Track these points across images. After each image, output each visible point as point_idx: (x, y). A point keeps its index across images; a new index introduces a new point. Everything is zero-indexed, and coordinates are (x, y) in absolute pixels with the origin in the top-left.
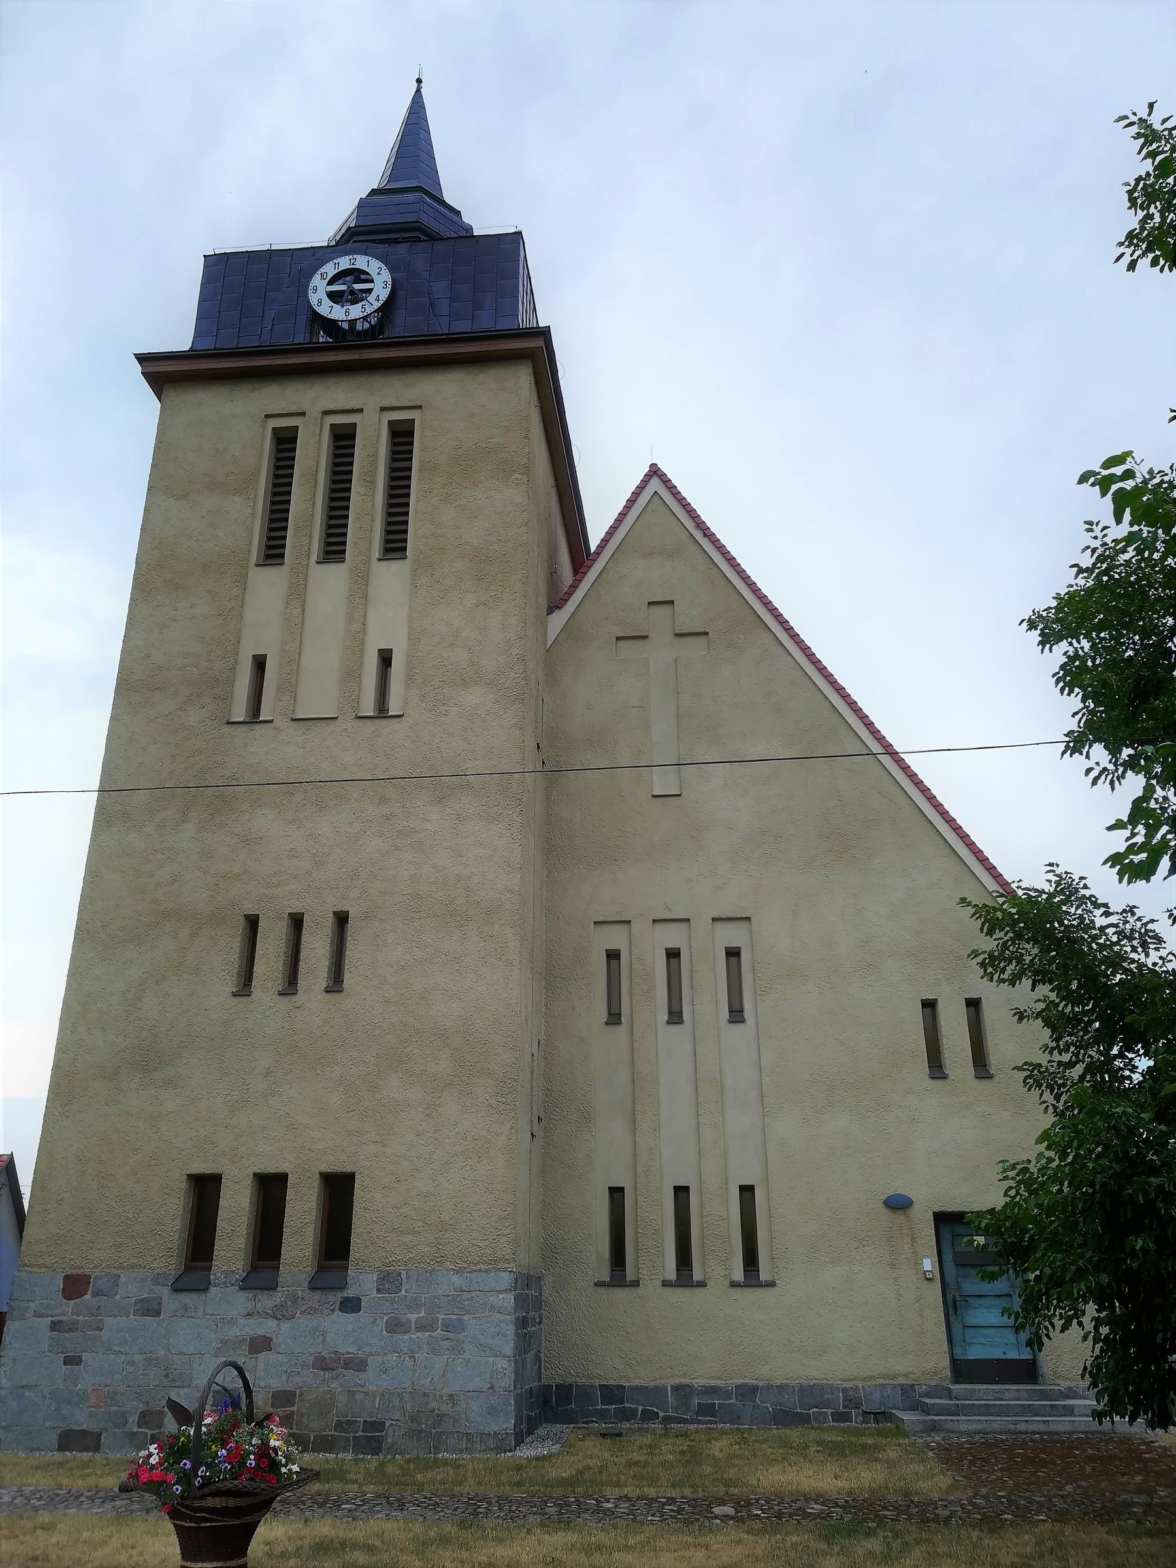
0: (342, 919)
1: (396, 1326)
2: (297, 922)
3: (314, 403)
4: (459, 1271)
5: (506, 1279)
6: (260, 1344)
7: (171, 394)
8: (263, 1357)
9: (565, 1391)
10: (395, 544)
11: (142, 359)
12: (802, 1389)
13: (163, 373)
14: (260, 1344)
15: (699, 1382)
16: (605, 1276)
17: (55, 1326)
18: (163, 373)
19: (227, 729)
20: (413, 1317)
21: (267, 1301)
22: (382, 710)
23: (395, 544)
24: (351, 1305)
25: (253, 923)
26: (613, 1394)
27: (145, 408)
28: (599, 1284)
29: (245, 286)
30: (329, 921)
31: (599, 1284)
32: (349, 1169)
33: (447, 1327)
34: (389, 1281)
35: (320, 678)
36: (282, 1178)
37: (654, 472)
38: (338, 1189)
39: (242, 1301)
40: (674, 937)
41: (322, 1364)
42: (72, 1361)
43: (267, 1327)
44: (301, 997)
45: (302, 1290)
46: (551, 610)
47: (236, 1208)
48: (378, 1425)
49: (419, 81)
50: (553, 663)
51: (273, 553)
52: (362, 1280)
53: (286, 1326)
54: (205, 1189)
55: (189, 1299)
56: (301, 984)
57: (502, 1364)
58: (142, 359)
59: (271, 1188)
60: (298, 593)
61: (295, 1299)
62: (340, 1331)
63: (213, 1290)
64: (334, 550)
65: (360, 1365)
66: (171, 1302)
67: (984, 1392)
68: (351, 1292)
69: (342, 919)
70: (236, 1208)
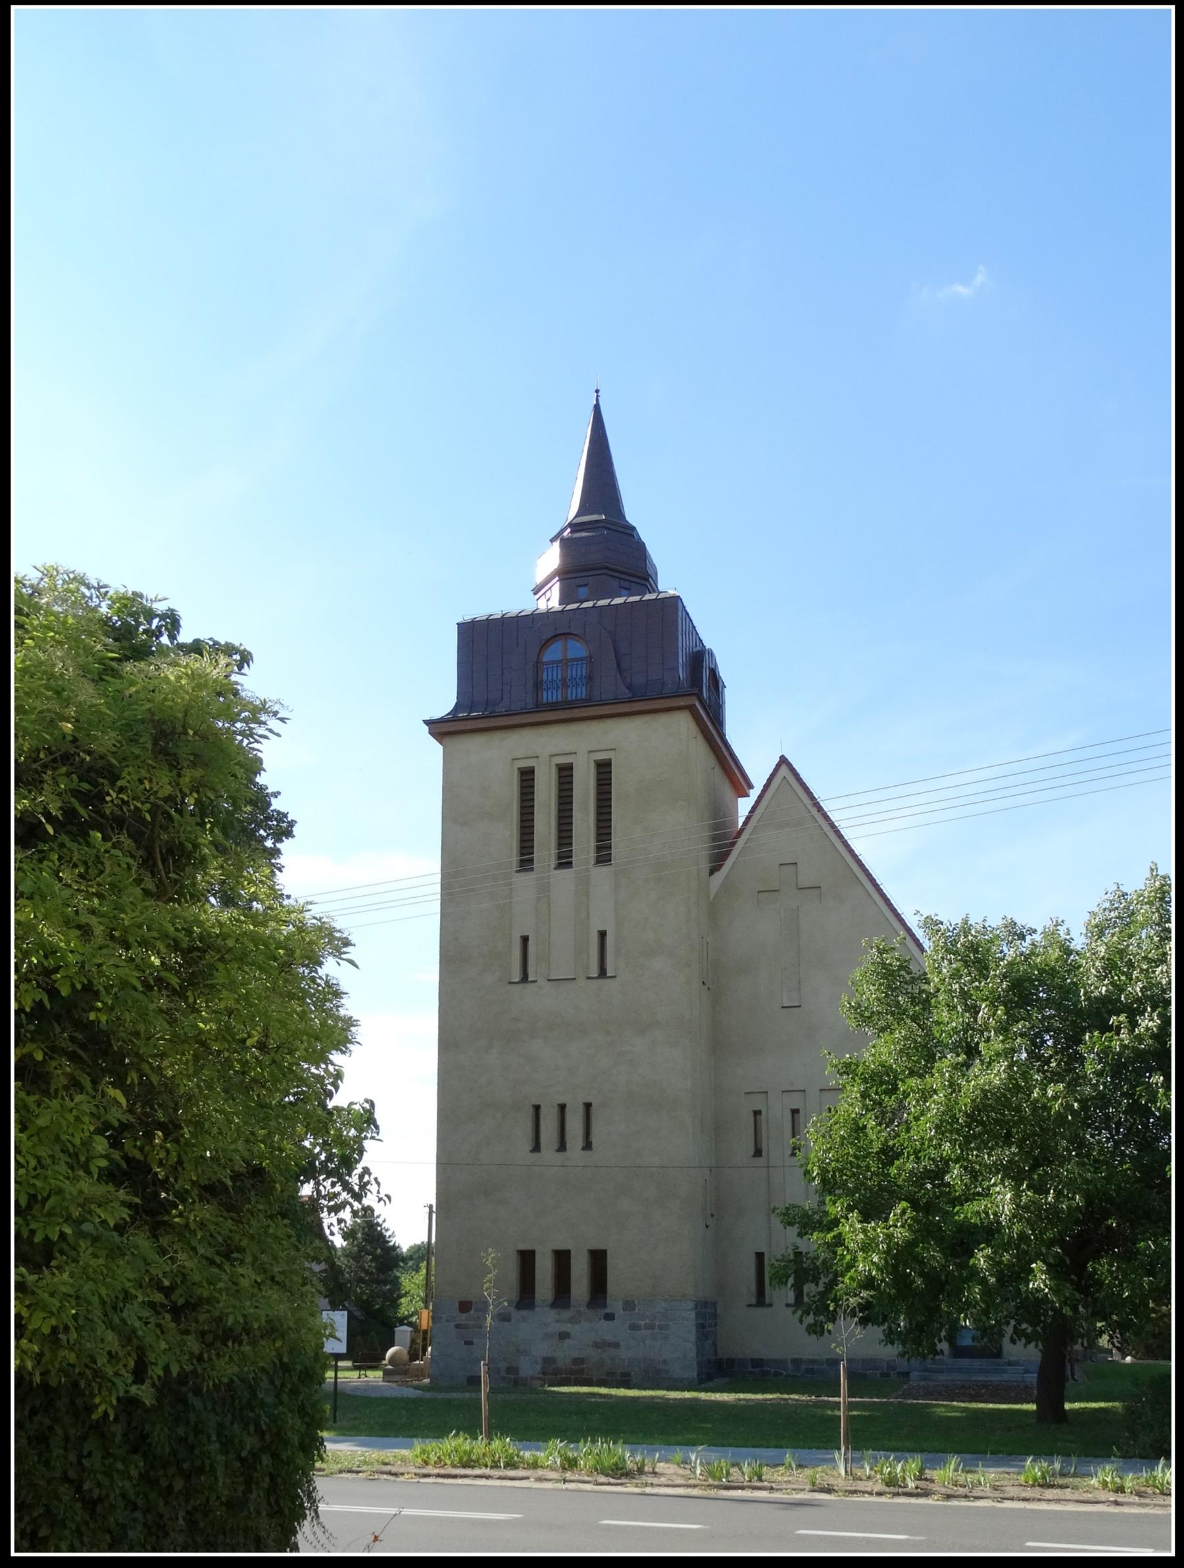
0: (588, 1106)
1: (634, 1327)
2: (562, 1108)
3: (544, 746)
4: (665, 1300)
5: (691, 1305)
6: (564, 1336)
7: (447, 740)
8: (567, 1341)
9: (731, 1362)
10: (603, 855)
11: (427, 722)
12: (863, 1360)
13: (440, 729)
14: (564, 1336)
15: (804, 1357)
16: (753, 1301)
17: (457, 1326)
18: (440, 729)
19: (509, 987)
20: (642, 1323)
21: (566, 1314)
22: (603, 973)
23: (603, 855)
24: (610, 1317)
25: (537, 1108)
26: (758, 1363)
27: (434, 750)
28: (750, 1306)
29: (487, 646)
30: (581, 1110)
31: (750, 1306)
32: (603, 1247)
33: (661, 1327)
34: (629, 1305)
35: (562, 951)
36: (568, 1252)
37: (783, 761)
38: (598, 1259)
39: (551, 1315)
40: (795, 1102)
41: (596, 1345)
42: (469, 1343)
43: (567, 1327)
44: (569, 1152)
45: (583, 1309)
46: (712, 872)
47: (544, 1269)
48: (627, 1374)
49: (597, 391)
50: (715, 912)
51: (526, 862)
52: (615, 1304)
53: (577, 1327)
54: (527, 1259)
55: (524, 1313)
56: (568, 1146)
57: (690, 1345)
58: (427, 722)
59: (562, 1259)
60: (544, 890)
61: (579, 1313)
62: (605, 1330)
63: (537, 1309)
64: (564, 861)
65: (616, 1345)
66: (516, 1315)
67: (964, 1362)
68: (608, 1310)
69: (588, 1106)
70: (544, 1269)
